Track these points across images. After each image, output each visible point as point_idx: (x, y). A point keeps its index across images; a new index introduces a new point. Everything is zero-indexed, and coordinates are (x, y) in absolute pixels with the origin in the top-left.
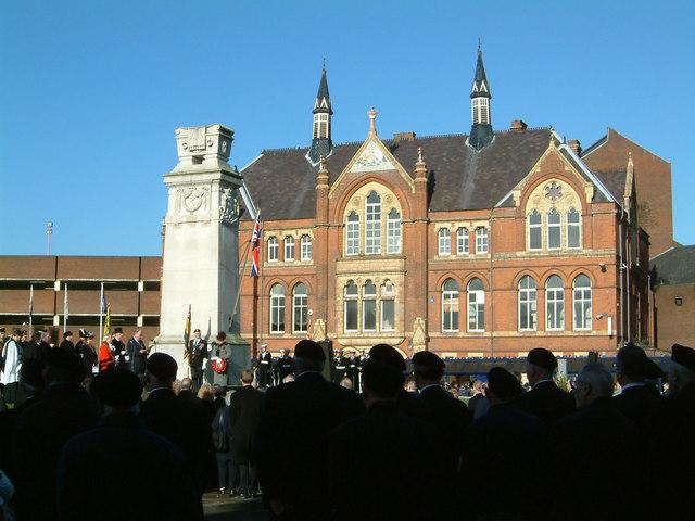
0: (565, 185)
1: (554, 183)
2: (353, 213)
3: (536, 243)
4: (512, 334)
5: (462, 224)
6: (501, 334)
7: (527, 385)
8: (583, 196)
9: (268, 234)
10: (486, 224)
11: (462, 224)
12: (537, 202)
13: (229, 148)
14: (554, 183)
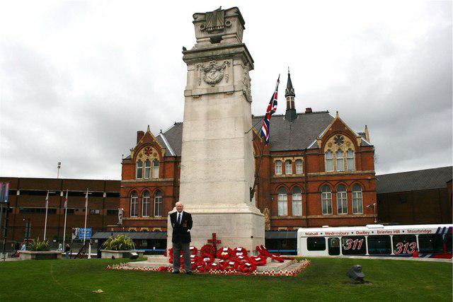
0: (345, 137)
1: (339, 136)
2: (140, 160)
3: (140, 176)
4: (319, 216)
5: (288, 158)
6: (313, 217)
7: (195, 251)
8: (160, 154)
9: (275, 159)
10: (302, 158)
11: (288, 158)
12: (330, 146)
13: (269, 108)
14: (339, 136)
